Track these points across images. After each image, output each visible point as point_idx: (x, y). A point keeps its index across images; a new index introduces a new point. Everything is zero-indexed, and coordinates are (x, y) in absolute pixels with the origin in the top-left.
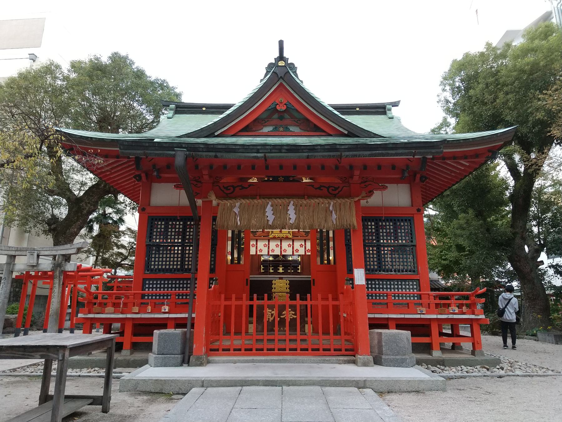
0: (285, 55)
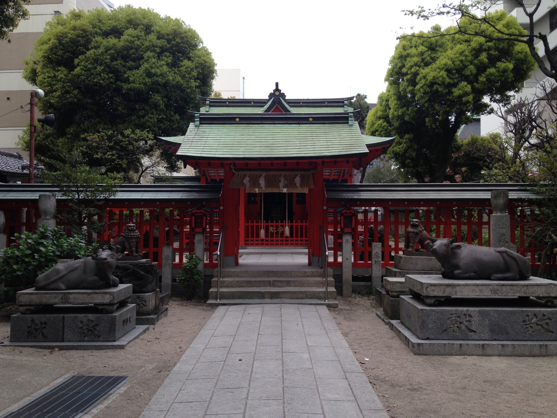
0: (279, 88)
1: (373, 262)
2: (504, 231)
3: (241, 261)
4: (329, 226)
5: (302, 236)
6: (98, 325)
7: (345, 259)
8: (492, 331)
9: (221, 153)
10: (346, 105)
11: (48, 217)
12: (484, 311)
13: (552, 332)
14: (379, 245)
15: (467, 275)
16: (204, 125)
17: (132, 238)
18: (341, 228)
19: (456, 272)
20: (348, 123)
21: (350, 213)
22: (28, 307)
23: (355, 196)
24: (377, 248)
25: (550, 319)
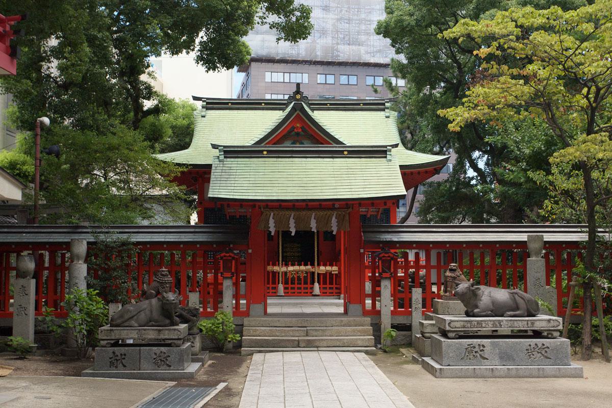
1: (413, 308)
2: (539, 275)
3: (269, 310)
4: (366, 298)
5: (331, 283)
6: (169, 356)
7: (383, 306)
8: (501, 358)
9: (254, 194)
10: (388, 108)
11: (80, 262)
12: (494, 342)
13: (550, 359)
14: (420, 290)
15: (484, 313)
16: (228, 159)
17: (166, 283)
18: (379, 273)
19: (476, 311)
20: (386, 157)
21: (389, 257)
22: (108, 341)
23: (395, 238)
24: (417, 294)
25: (548, 348)
